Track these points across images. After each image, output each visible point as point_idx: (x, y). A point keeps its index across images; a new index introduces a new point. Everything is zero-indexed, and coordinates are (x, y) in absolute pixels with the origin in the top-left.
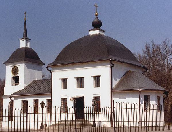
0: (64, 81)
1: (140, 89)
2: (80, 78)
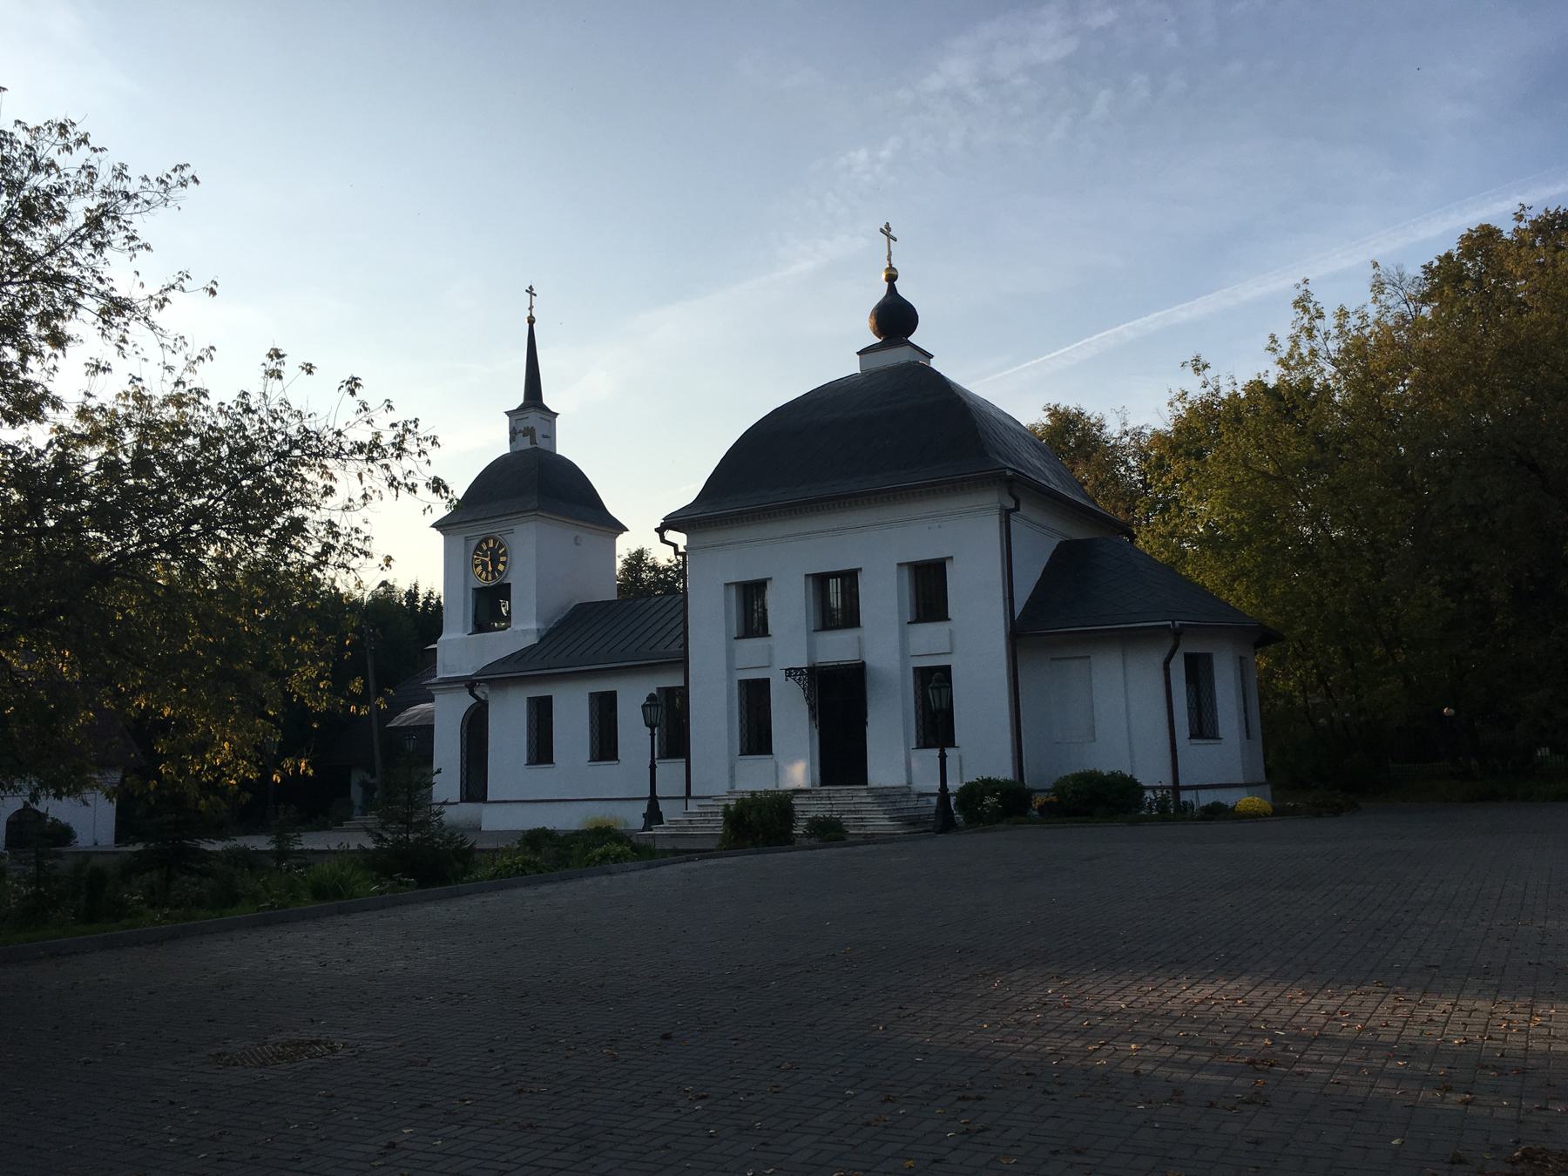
0: (751, 595)
1: (1173, 621)
2: (838, 628)
